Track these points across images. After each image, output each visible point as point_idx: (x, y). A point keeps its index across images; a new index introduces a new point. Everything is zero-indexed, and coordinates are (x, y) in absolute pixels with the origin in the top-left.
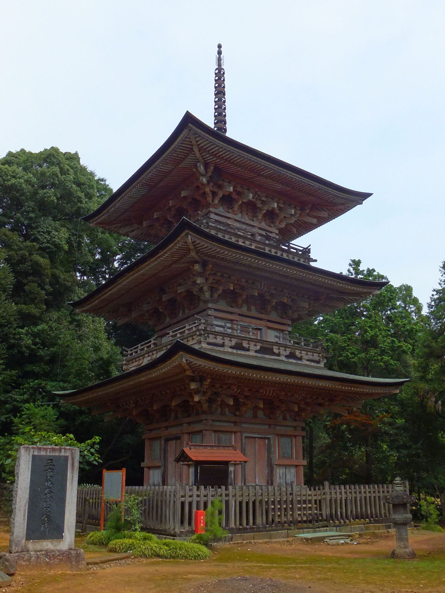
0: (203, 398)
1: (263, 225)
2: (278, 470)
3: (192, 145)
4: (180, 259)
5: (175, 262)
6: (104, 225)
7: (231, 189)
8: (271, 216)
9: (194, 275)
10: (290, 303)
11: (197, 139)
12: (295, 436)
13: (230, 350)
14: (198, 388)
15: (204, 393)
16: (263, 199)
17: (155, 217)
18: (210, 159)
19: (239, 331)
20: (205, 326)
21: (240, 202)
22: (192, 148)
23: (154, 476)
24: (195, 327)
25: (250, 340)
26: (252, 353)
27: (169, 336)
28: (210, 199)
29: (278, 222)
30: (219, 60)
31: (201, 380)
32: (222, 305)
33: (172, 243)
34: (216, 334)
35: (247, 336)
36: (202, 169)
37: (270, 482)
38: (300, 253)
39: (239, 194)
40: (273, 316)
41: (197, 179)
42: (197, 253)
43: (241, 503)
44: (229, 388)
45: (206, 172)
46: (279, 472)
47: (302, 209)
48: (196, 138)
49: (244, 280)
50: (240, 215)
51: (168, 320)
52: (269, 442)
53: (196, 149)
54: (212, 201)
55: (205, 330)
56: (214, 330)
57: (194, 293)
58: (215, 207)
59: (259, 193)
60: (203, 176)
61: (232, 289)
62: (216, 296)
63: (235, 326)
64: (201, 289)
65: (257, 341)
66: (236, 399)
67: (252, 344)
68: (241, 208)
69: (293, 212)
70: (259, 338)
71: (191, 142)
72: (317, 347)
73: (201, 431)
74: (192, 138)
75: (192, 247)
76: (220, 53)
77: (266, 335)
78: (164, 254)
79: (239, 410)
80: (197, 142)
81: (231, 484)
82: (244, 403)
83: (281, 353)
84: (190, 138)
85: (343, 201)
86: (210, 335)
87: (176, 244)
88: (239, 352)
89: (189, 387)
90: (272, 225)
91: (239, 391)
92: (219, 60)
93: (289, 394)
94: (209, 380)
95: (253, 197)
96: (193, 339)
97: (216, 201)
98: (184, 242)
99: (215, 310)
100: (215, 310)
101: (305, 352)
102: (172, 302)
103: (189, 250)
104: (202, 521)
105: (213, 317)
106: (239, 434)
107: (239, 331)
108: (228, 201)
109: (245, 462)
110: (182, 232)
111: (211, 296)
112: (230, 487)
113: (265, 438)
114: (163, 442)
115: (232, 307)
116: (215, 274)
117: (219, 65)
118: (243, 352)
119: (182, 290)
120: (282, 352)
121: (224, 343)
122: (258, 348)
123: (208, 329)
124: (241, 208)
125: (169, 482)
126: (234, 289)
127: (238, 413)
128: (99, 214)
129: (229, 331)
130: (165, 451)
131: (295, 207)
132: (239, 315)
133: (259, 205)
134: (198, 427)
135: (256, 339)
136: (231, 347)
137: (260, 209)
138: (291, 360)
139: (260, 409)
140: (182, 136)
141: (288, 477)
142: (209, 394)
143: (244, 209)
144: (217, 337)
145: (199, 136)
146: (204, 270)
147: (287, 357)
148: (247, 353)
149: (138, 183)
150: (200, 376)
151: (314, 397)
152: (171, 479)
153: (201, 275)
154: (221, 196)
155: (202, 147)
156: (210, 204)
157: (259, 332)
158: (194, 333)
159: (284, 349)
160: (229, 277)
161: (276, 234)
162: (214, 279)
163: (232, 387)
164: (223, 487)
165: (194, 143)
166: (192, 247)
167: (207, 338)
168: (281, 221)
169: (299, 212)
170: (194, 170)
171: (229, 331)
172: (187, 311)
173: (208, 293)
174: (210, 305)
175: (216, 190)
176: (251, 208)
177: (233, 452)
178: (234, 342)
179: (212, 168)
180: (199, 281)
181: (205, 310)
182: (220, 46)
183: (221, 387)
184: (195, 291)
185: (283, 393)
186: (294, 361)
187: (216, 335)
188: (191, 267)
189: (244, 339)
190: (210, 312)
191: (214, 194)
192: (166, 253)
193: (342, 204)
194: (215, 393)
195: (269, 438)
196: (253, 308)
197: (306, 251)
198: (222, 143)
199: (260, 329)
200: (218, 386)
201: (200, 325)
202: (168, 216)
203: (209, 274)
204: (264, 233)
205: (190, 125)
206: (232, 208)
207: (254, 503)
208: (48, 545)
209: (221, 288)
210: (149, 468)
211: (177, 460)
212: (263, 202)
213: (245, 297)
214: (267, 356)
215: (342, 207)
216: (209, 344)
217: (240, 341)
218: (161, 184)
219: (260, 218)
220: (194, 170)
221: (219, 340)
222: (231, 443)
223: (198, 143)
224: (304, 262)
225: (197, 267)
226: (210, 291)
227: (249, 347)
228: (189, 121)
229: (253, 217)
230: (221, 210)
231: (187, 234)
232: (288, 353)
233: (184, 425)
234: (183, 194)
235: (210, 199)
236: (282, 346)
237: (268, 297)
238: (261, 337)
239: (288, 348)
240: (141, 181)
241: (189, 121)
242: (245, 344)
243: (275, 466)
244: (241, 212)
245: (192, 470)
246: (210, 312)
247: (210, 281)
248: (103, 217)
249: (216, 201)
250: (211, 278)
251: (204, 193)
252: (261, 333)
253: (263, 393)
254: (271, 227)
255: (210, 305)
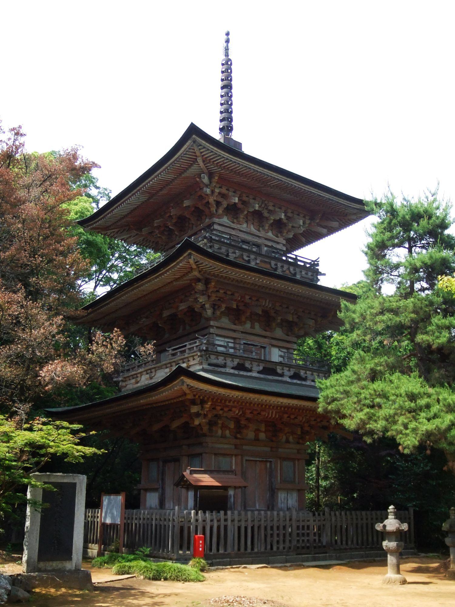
0: (204, 421)
1: (270, 234)
2: (279, 495)
3: (196, 156)
4: (182, 277)
5: (177, 280)
6: (99, 230)
7: (236, 200)
8: (278, 226)
9: (196, 292)
10: (296, 320)
11: (201, 151)
12: (298, 460)
13: (232, 371)
14: (198, 412)
15: (205, 416)
16: (271, 208)
17: (155, 225)
18: (215, 169)
19: (241, 351)
20: (206, 346)
21: (246, 212)
22: (196, 159)
23: (152, 499)
24: (197, 346)
25: (252, 360)
26: (255, 374)
27: (168, 354)
28: (213, 209)
29: (285, 232)
30: (227, 49)
31: (203, 402)
32: (225, 322)
33: (174, 261)
34: (218, 354)
35: (250, 356)
36: (206, 180)
37: (271, 505)
38: (308, 266)
39: (244, 203)
40: (279, 333)
41: (201, 189)
42: (200, 272)
43: (239, 528)
44: (230, 410)
45: (210, 182)
46: (281, 496)
47: (312, 219)
48: (200, 149)
49: (247, 297)
50: (245, 225)
51: (167, 336)
52: (271, 466)
53: (200, 160)
54: (216, 211)
55: (207, 350)
56: (216, 350)
57: (196, 309)
58: (219, 217)
59: (266, 202)
60: (207, 186)
61: (235, 307)
62: (218, 313)
63: (237, 346)
64: (203, 306)
65: (259, 361)
66: (237, 421)
67: (255, 364)
68: (247, 218)
69: (301, 222)
70: (263, 358)
71: (195, 153)
72: (323, 366)
73: (201, 454)
74: (196, 149)
75: (194, 266)
76: (227, 41)
77: (270, 353)
78: (165, 272)
79: (240, 433)
80: (201, 153)
81: (231, 509)
82: (246, 426)
83: (285, 374)
84: (194, 149)
85: (355, 211)
86: (211, 356)
87: (178, 264)
88: (242, 373)
89: (190, 411)
90: (279, 235)
91: (241, 413)
92: (227, 49)
93: (292, 417)
94: (209, 403)
95: (260, 207)
96: (194, 359)
97: (220, 211)
98: (186, 262)
99: (217, 327)
100: (217, 327)
101: (311, 373)
102: (173, 318)
103: (192, 269)
104: (201, 546)
105: (215, 335)
106: (240, 457)
107: (241, 351)
108: (233, 211)
109: (245, 487)
110: (185, 252)
111: (214, 313)
112: (229, 513)
113: (266, 461)
114: (161, 463)
115: (235, 324)
116: (218, 291)
117: (227, 55)
118: (245, 373)
119: (183, 307)
120: (287, 373)
121: (225, 363)
122: (261, 368)
123: (209, 349)
124: (247, 218)
125: (167, 506)
126: (237, 306)
127: (239, 436)
128: (95, 219)
129: (232, 351)
130: (163, 473)
131: (304, 217)
132: (242, 332)
133: (266, 214)
134: (198, 450)
135: (259, 359)
136: (233, 368)
137: (267, 219)
138: (295, 381)
139: (262, 432)
140: (185, 147)
141: (290, 502)
142: (210, 416)
143: (249, 218)
144: (219, 357)
145: (204, 148)
146: (207, 287)
147: (291, 377)
148: (249, 374)
149: (139, 190)
150: (201, 399)
151: (318, 420)
152: (169, 504)
153: (203, 293)
154: (225, 206)
155: (206, 158)
156: (214, 214)
157: (263, 350)
158: (195, 354)
159: (288, 369)
160: (232, 294)
161: (284, 245)
162: (216, 297)
163: (234, 409)
164: (222, 512)
165: (198, 154)
166: (194, 266)
167: (209, 359)
168: (289, 231)
169: (308, 222)
170: (198, 179)
171: (232, 351)
172: (188, 327)
173: (210, 311)
174: (212, 323)
175: (220, 199)
176: (258, 217)
177: (234, 476)
178: (236, 361)
179: (216, 178)
180: (202, 299)
181: (206, 328)
182: (228, 34)
183: (222, 409)
184: (197, 307)
185: (286, 416)
186: (299, 382)
187: (218, 356)
188: (193, 284)
189: (247, 358)
190: (212, 330)
191: (218, 204)
192: (167, 271)
193: (355, 214)
194: (216, 416)
195: (271, 462)
196: (257, 325)
197: (315, 264)
198: (227, 155)
199: (264, 348)
200: (219, 408)
201: (201, 345)
202: (169, 224)
203: (212, 291)
204: (270, 244)
205: (194, 136)
206: (237, 218)
207: (253, 528)
208: (55, 565)
209: (224, 306)
210: (146, 490)
211: (177, 484)
212: (270, 212)
213: (248, 314)
214: (270, 377)
215: (354, 217)
216: (209, 365)
217: (241, 362)
218: (161, 193)
219: (267, 228)
220: (198, 179)
221: (221, 361)
222: (231, 467)
223: (202, 154)
224: (312, 275)
225: (200, 286)
226: (212, 309)
227: (251, 367)
228: (193, 131)
229: (260, 226)
230: (225, 220)
231: (190, 254)
232: (292, 373)
233: (184, 447)
234: (186, 203)
235: (213, 209)
236: (286, 367)
237: (272, 314)
238: (265, 357)
239: (293, 368)
240: (141, 189)
241: (193, 131)
242: (247, 365)
243: (276, 490)
244: (247, 222)
245: (191, 494)
246: (212, 330)
247: (213, 298)
248: (100, 222)
249: (220, 211)
250: (214, 295)
251: (208, 203)
252: (265, 352)
253: (265, 415)
254: (278, 237)
255: (212, 323)
